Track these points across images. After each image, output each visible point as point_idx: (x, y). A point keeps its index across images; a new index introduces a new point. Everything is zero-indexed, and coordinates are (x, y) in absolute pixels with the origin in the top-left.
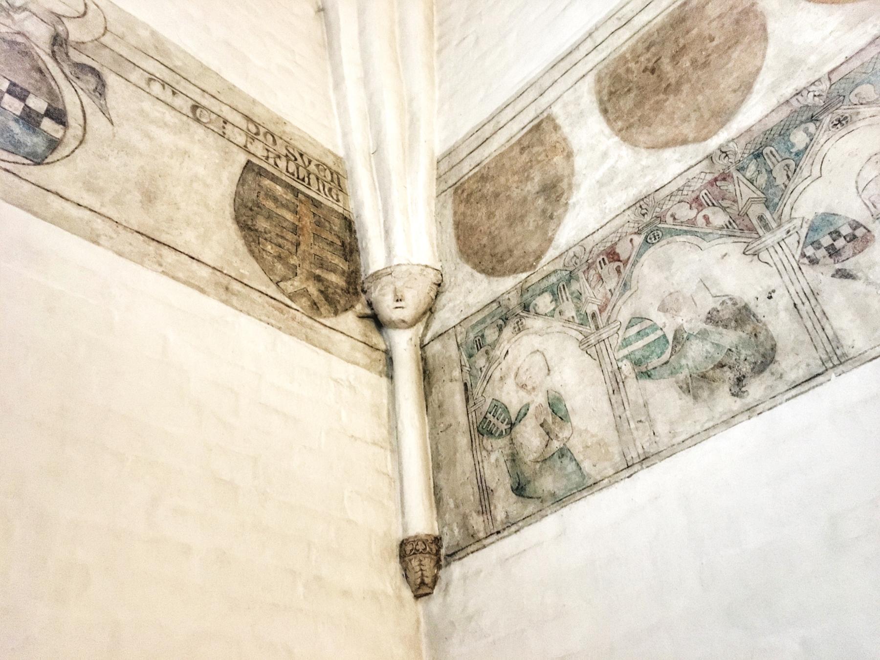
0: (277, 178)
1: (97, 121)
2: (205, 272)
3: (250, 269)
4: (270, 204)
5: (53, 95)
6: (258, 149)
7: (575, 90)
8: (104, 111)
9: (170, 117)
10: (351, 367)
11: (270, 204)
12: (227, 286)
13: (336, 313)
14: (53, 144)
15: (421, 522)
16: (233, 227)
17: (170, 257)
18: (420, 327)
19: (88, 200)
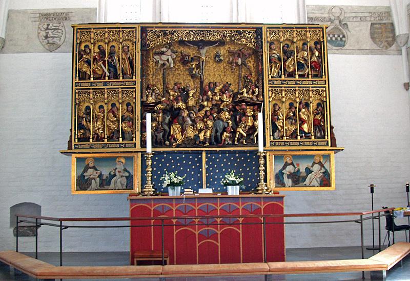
0: (141, 141)
1: (349, 33)
2: (367, 51)
3: (375, 47)
4: (376, 30)
5: (342, 33)
6: (372, 19)
7: (371, 229)
8: (349, 31)
9: (357, 24)
10: (395, 56)
11: (376, 30)
12: (371, 52)
13: (391, 46)
14: (345, 42)
15: (406, 81)
16: (370, 39)
17: (362, 51)
18: (406, 45)
19: (351, 48)
